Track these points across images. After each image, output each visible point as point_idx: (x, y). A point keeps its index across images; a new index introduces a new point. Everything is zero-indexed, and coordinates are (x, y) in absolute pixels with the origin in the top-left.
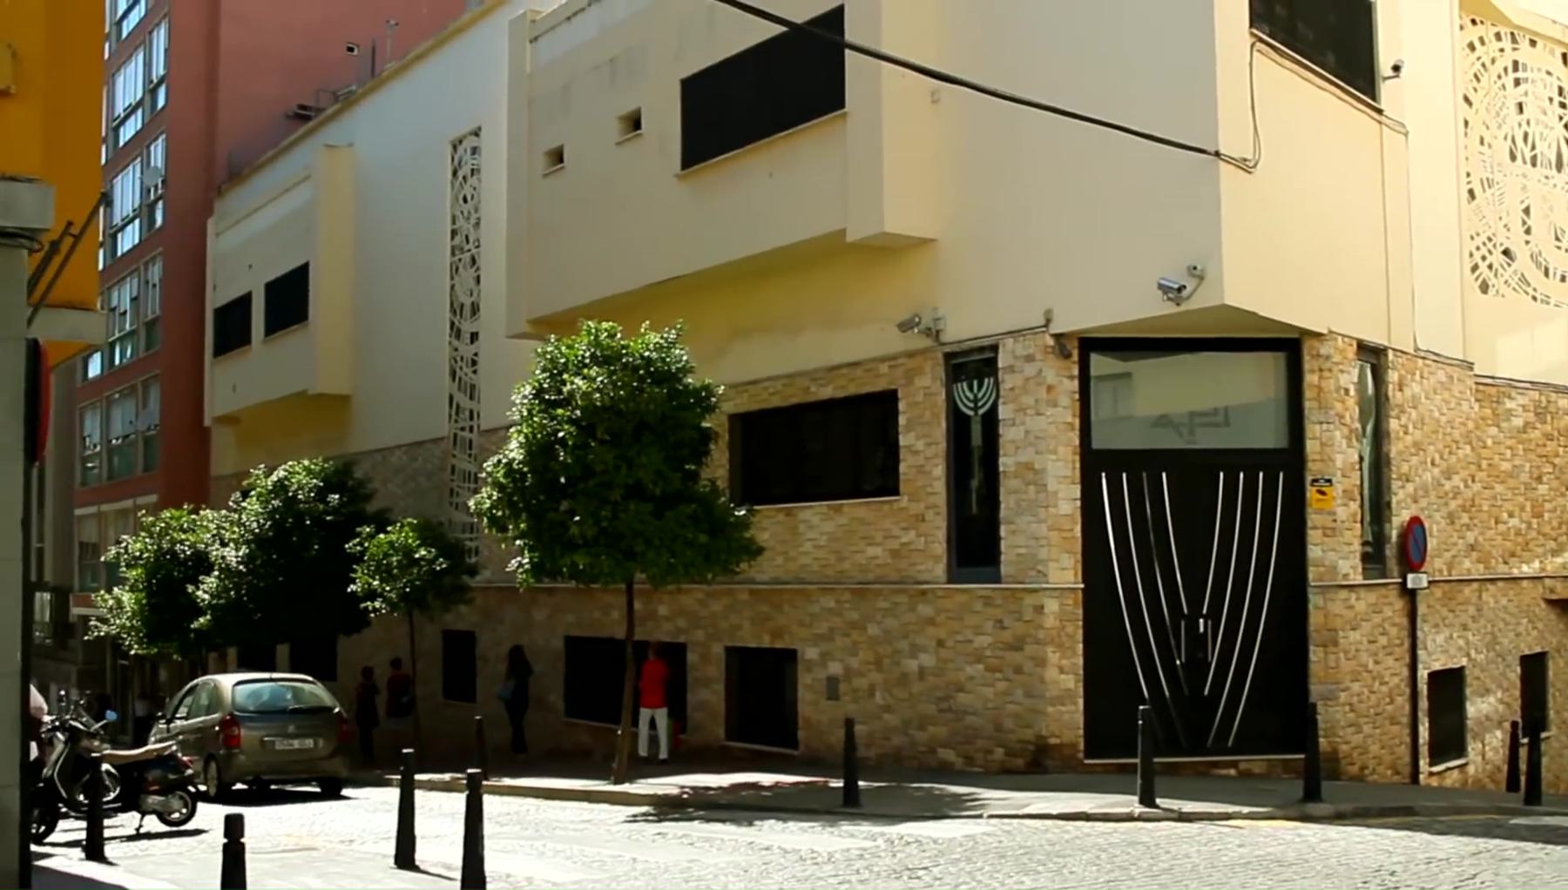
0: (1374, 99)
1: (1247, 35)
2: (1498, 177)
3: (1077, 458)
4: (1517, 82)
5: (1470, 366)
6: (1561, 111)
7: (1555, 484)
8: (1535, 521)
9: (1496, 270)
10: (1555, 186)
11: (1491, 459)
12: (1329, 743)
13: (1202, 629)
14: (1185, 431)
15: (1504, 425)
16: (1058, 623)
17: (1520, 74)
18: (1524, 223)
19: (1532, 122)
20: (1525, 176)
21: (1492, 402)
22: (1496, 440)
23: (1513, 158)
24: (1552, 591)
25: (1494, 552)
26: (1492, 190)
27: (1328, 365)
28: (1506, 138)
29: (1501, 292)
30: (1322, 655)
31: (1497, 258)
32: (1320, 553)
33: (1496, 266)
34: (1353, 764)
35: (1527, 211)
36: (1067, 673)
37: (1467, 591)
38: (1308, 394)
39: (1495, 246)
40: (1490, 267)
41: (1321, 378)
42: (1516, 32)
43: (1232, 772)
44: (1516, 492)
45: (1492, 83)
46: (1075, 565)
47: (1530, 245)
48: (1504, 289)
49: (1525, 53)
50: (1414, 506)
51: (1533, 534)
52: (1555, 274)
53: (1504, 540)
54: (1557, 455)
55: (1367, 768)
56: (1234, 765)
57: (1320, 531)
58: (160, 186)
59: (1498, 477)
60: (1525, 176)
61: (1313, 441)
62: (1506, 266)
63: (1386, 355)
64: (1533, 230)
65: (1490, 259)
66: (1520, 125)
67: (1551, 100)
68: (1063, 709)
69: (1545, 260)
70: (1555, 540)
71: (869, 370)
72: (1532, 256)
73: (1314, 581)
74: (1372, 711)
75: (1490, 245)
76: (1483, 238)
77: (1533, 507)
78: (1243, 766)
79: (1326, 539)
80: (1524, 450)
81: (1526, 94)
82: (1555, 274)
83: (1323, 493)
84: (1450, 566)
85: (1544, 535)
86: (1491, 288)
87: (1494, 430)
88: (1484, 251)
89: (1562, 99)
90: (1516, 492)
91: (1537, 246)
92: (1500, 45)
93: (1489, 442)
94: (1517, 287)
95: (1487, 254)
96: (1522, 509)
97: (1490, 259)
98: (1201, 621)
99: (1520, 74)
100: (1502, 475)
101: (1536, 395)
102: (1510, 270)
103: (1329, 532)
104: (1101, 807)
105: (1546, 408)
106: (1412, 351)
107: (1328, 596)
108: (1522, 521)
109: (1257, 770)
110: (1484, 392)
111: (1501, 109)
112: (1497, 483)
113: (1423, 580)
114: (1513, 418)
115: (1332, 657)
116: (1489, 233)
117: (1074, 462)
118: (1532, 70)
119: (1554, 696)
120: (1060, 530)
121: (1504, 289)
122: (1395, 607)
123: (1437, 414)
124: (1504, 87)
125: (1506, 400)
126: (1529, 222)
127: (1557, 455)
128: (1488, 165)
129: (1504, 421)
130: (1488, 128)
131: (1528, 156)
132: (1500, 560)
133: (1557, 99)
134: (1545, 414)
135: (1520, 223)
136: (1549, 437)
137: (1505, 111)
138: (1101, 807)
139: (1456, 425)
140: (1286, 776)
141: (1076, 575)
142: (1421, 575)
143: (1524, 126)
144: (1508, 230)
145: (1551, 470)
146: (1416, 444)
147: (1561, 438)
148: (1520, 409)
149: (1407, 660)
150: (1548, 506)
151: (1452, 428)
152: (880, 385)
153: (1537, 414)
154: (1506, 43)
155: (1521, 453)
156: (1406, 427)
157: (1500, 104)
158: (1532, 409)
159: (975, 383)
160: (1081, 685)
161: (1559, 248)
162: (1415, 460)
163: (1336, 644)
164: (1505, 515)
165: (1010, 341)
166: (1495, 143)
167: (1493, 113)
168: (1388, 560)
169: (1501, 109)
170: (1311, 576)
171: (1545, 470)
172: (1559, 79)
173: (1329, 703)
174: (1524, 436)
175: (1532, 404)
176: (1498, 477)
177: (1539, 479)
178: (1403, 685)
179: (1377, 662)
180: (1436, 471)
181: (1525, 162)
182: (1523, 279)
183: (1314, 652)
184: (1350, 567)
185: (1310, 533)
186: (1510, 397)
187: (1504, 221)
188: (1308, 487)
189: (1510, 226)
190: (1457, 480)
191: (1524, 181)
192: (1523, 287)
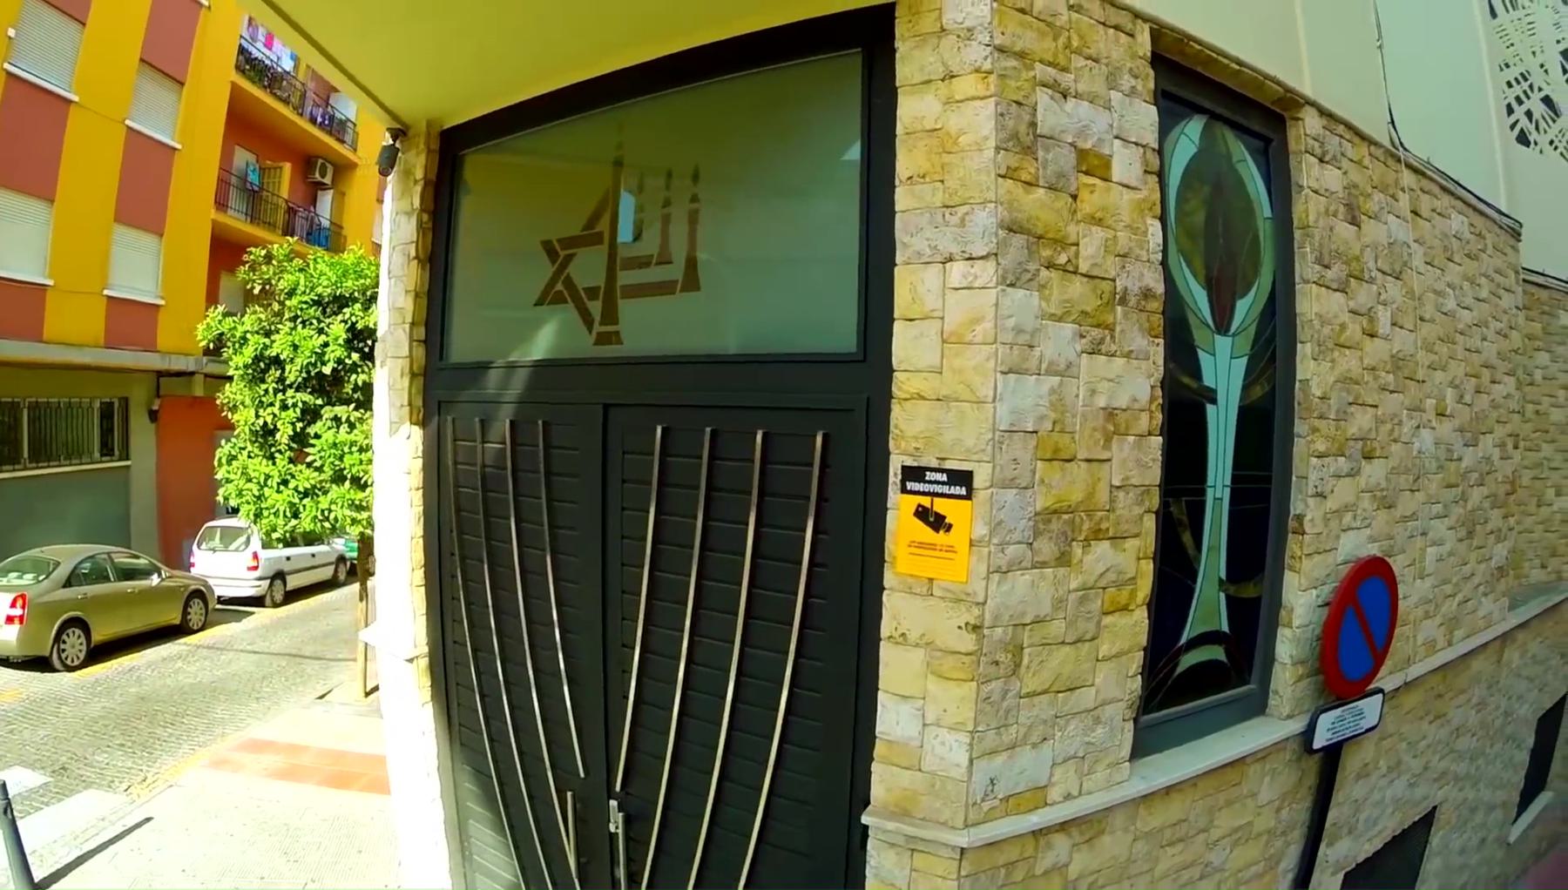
11: (1539, 404)
14: (595, 308)
31: (1539, 109)
33: (1536, 115)
40: (943, 743)
50: (1382, 515)
75: (1525, 86)
79: (933, 685)
83: (938, 523)
93: (1538, 375)
100: (1552, 428)
106: (1387, 143)
139: (1491, 334)
146: (1397, 362)
156: (1370, 315)
162: (1392, 403)
164: (1551, 493)
180: (1446, 428)
188: (894, 496)
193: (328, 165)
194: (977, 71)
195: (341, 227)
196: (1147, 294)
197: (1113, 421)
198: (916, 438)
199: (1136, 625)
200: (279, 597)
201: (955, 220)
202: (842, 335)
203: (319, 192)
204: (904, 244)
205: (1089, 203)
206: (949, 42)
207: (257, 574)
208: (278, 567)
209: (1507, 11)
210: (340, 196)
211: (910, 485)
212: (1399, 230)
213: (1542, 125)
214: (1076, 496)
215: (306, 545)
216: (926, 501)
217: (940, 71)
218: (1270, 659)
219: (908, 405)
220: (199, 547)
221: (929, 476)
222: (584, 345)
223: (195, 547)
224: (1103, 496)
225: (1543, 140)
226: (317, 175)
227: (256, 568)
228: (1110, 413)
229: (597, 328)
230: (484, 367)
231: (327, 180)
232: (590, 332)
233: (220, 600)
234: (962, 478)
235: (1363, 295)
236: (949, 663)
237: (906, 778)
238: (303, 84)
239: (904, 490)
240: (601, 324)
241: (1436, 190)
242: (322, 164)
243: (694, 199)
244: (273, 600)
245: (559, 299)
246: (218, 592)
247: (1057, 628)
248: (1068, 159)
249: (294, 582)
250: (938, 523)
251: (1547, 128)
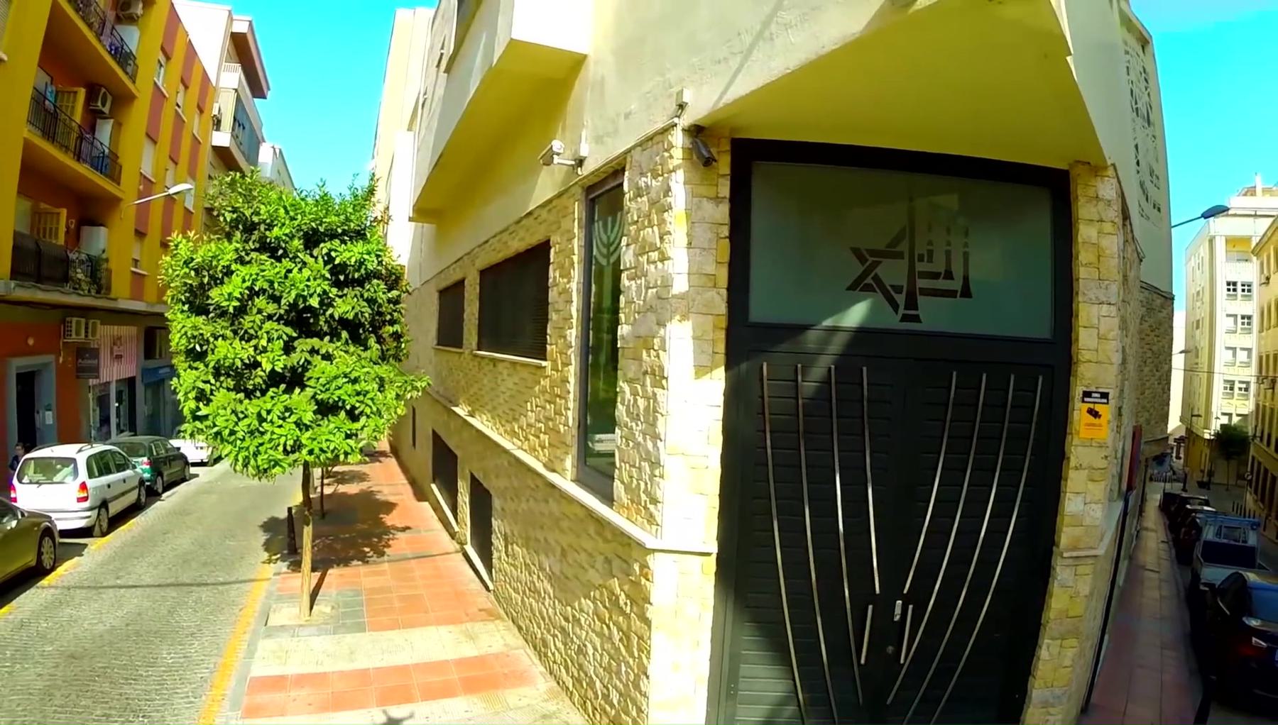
3: (722, 335)
14: (901, 299)
79: (1091, 486)
83: (1095, 414)
98: (899, 602)
104: (173, 494)
138: (173, 494)
152: (533, 239)
159: (610, 219)
193: (108, 95)
194: (1112, 222)
195: (118, 157)
198: (1089, 379)
200: (105, 525)
201: (1103, 286)
202: (1041, 329)
203: (98, 121)
204: (1084, 293)
206: (1101, 205)
207: (87, 504)
208: (102, 496)
210: (118, 126)
211: (1086, 399)
215: (118, 471)
216: (1091, 406)
217: (1096, 217)
219: (1085, 364)
220: (20, 481)
221: (1094, 395)
222: (892, 320)
223: (15, 481)
226: (99, 104)
227: (85, 499)
229: (901, 311)
230: (805, 328)
231: (106, 110)
232: (897, 313)
233: (66, 533)
234: (1105, 396)
236: (1097, 475)
237: (1078, 531)
238: (104, 13)
239: (1083, 401)
240: (906, 308)
242: (105, 93)
243: (949, 244)
244: (101, 530)
245: (868, 288)
246: (61, 526)
249: (115, 508)
250: (1095, 414)
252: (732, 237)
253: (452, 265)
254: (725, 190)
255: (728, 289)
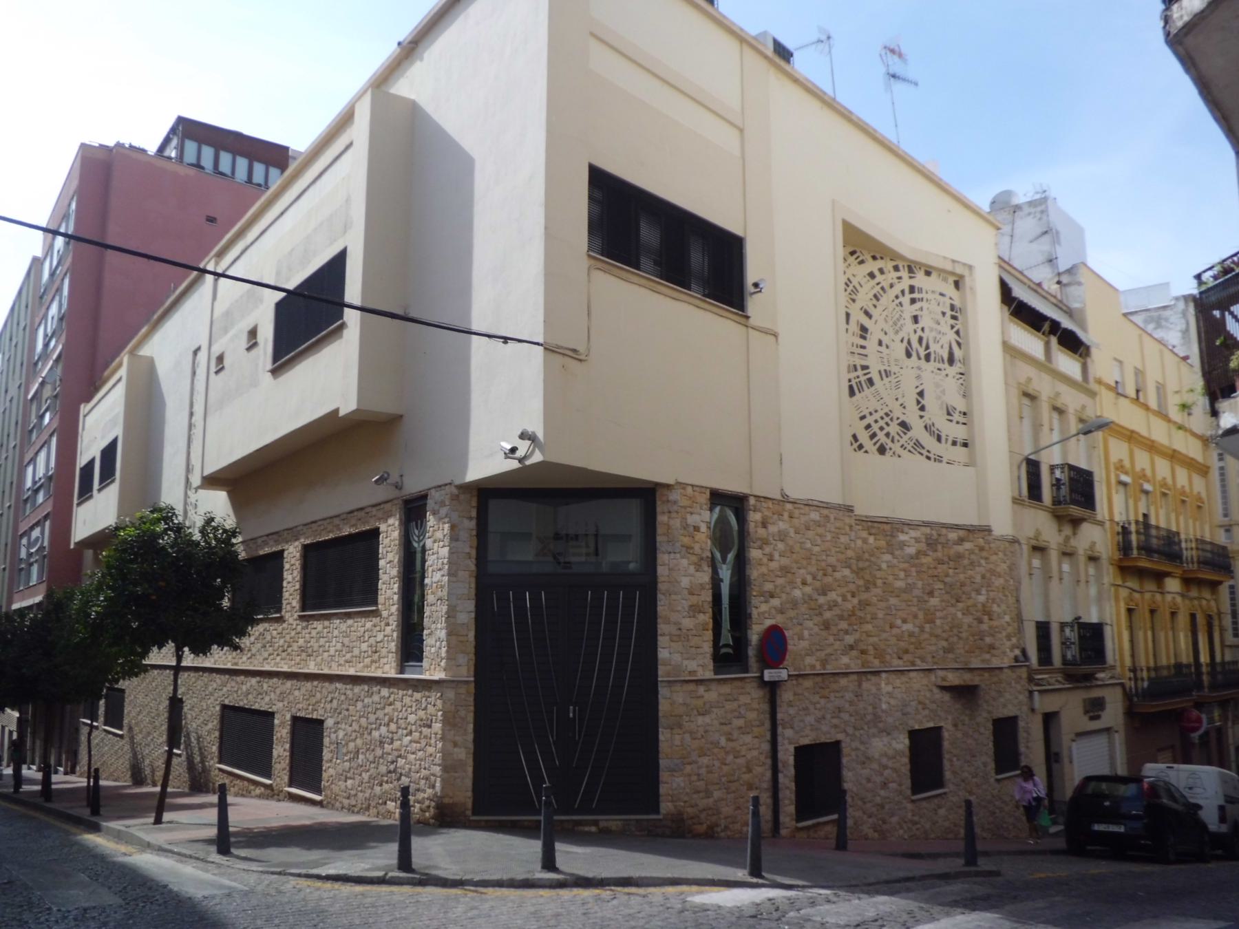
0: (743, 311)
1: (585, 257)
2: (894, 369)
3: (473, 580)
4: (913, 301)
5: (849, 509)
6: (953, 322)
7: (947, 597)
8: (927, 625)
9: (893, 438)
10: (947, 375)
12: (675, 807)
13: (571, 715)
15: (897, 553)
16: (453, 707)
17: (916, 295)
18: (918, 402)
19: (926, 330)
20: (919, 368)
21: (887, 535)
22: (890, 564)
23: (909, 355)
24: (944, 679)
25: (889, 651)
26: (889, 379)
27: (675, 508)
28: (902, 341)
29: (896, 453)
30: (669, 735)
31: (894, 429)
32: (668, 655)
34: (701, 824)
35: (921, 394)
36: (460, 747)
37: (843, 682)
38: (660, 530)
39: (891, 419)
41: (669, 518)
42: (913, 266)
43: (593, 829)
44: (910, 603)
45: (890, 302)
46: (468, 662)
47: (923, 419)
48: (900, 451)
49: (920, 280)
51: (926, 636)
52: (947, 440)
53: (898, 640)
54: (947, 575)
55: (717, 825)
56: (596, 823)
57: (668, 638)
58: (58, 383)
59: (892, 592)
60: (919, 368)
61: (663, 567)
62: (902, 434)
63: (748, 501)
64: (927, 408)
65: (887, 429)
66: (915, 332)
67: (944, 314)
68: (456, 775)
69: (938, 430)
70: (947, 640)
71: (367, 513)
72: (926, 427)
73: (662, 677)
74: (724, 779)
75: (887, 419)
76: (881, 413)
77: (926, 614)
78: (602, 824)
79: (672, 644)
80: (917, 572)
81: (921, 309)
82: (947, 440)
84: (824, 663)
85: (937, 636)
86: (888, 450)
87: (887, 557)
88: (882, 423)
89: (953, 313)
90: (910, 603)
91: (930, 419)
92: (898, 274)
93: (884, 566)
94: (912, 449)
95: (885, 426)
96: (915, 616)
97: (887, 429)
99: (916, 295)
101: (928, 530)
102: (906, 438)
103: (675, 638)
105: (937, 540)
107: (673, 689)
108: (915, 626)
109: (614, 828)
110: (879, 528)
111: (898, 320)
112: (891, 596)
113: (783, 674)
114: (906, 548)
115: (677, 737)
116: (886, 410)
117: (470, 583)
118: (927, 293)
119: (951, 761)
120: (457, 635)
121: (900, 451)
122: (752, 697)
123: (809, 545)
124: (901, 304)
125: (900, 534)
126: (923, 402)
127: (947, 575)
128: (885, 360)
129: (897, 550)
130: (886, 334)
131: (922, 353)
132: (895, 655)
133: (949, 313)
134: (936, 545)
135: (915, 402)
136: (941, 562)
137: (902, 322)
140: (638, 833)
141: (468, 670)
142: (781, 670)
143: (919, 333)
144: (904, 407)
145: (942, 587)
147: (951, 562)
148: (913, 541)
149: (768, 736)
150: (939, 614)
151: (827, 556)
153: (928, 545)
154: (904, 273)
155: (915, 574)
157: (897, 316)
158: (924, 540)
160: (471, 756)
161: (951, 421)
162: (780, 581)
163: (680, 726)
164: (899, 622)
165: (433, 492)
166: (892, 345)
167: (891, 323)
168: (749, 659)
169: (898, 320)
170: (660, 673)
171: (936, 587)
172: (951, 298)
173: (675, 774)
174: (916, 561)
175: (923, 536)
176: (892, 592)
177: (931, 594)
178: (762, 758)
179: (729, 740)
180: (808, 589)
181: (919, 358)
182: (918, 444)
183: (663, 733)
184: (702, 665)
185: (660, 638)
186: (902, 532)
187: (900, 401)
189: (905, 404)
190: (833, 595)
191: (919, 372)
192: (918, 450)
196: (708, 557)
197: (702, 586)
199: (709, 635)
205: (697, 538)
209: (882, 379)
212: (782, 525)
213: (897, 437)
214: (695, 602)
218: (747, 657)
224: (700, 603)
225: (896, 447)
228: (701, 585)
235: (768, 549)
241: (802, 506)
247: (694, 632)
248: (692, 529)
251: (899, 439)
252: (478, 536)
253: (320, 520)
254: (474, 513)
255: (476, 559)
